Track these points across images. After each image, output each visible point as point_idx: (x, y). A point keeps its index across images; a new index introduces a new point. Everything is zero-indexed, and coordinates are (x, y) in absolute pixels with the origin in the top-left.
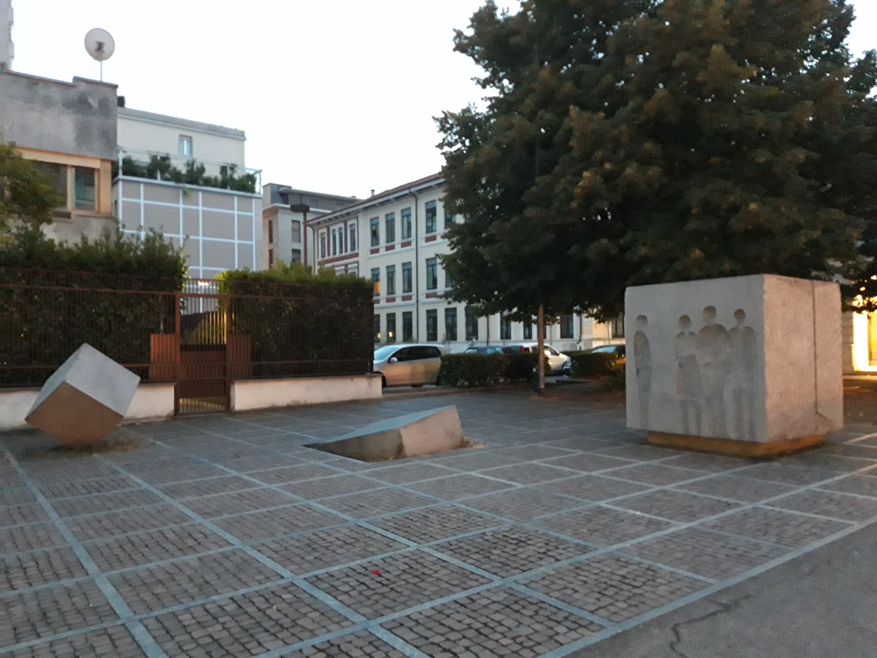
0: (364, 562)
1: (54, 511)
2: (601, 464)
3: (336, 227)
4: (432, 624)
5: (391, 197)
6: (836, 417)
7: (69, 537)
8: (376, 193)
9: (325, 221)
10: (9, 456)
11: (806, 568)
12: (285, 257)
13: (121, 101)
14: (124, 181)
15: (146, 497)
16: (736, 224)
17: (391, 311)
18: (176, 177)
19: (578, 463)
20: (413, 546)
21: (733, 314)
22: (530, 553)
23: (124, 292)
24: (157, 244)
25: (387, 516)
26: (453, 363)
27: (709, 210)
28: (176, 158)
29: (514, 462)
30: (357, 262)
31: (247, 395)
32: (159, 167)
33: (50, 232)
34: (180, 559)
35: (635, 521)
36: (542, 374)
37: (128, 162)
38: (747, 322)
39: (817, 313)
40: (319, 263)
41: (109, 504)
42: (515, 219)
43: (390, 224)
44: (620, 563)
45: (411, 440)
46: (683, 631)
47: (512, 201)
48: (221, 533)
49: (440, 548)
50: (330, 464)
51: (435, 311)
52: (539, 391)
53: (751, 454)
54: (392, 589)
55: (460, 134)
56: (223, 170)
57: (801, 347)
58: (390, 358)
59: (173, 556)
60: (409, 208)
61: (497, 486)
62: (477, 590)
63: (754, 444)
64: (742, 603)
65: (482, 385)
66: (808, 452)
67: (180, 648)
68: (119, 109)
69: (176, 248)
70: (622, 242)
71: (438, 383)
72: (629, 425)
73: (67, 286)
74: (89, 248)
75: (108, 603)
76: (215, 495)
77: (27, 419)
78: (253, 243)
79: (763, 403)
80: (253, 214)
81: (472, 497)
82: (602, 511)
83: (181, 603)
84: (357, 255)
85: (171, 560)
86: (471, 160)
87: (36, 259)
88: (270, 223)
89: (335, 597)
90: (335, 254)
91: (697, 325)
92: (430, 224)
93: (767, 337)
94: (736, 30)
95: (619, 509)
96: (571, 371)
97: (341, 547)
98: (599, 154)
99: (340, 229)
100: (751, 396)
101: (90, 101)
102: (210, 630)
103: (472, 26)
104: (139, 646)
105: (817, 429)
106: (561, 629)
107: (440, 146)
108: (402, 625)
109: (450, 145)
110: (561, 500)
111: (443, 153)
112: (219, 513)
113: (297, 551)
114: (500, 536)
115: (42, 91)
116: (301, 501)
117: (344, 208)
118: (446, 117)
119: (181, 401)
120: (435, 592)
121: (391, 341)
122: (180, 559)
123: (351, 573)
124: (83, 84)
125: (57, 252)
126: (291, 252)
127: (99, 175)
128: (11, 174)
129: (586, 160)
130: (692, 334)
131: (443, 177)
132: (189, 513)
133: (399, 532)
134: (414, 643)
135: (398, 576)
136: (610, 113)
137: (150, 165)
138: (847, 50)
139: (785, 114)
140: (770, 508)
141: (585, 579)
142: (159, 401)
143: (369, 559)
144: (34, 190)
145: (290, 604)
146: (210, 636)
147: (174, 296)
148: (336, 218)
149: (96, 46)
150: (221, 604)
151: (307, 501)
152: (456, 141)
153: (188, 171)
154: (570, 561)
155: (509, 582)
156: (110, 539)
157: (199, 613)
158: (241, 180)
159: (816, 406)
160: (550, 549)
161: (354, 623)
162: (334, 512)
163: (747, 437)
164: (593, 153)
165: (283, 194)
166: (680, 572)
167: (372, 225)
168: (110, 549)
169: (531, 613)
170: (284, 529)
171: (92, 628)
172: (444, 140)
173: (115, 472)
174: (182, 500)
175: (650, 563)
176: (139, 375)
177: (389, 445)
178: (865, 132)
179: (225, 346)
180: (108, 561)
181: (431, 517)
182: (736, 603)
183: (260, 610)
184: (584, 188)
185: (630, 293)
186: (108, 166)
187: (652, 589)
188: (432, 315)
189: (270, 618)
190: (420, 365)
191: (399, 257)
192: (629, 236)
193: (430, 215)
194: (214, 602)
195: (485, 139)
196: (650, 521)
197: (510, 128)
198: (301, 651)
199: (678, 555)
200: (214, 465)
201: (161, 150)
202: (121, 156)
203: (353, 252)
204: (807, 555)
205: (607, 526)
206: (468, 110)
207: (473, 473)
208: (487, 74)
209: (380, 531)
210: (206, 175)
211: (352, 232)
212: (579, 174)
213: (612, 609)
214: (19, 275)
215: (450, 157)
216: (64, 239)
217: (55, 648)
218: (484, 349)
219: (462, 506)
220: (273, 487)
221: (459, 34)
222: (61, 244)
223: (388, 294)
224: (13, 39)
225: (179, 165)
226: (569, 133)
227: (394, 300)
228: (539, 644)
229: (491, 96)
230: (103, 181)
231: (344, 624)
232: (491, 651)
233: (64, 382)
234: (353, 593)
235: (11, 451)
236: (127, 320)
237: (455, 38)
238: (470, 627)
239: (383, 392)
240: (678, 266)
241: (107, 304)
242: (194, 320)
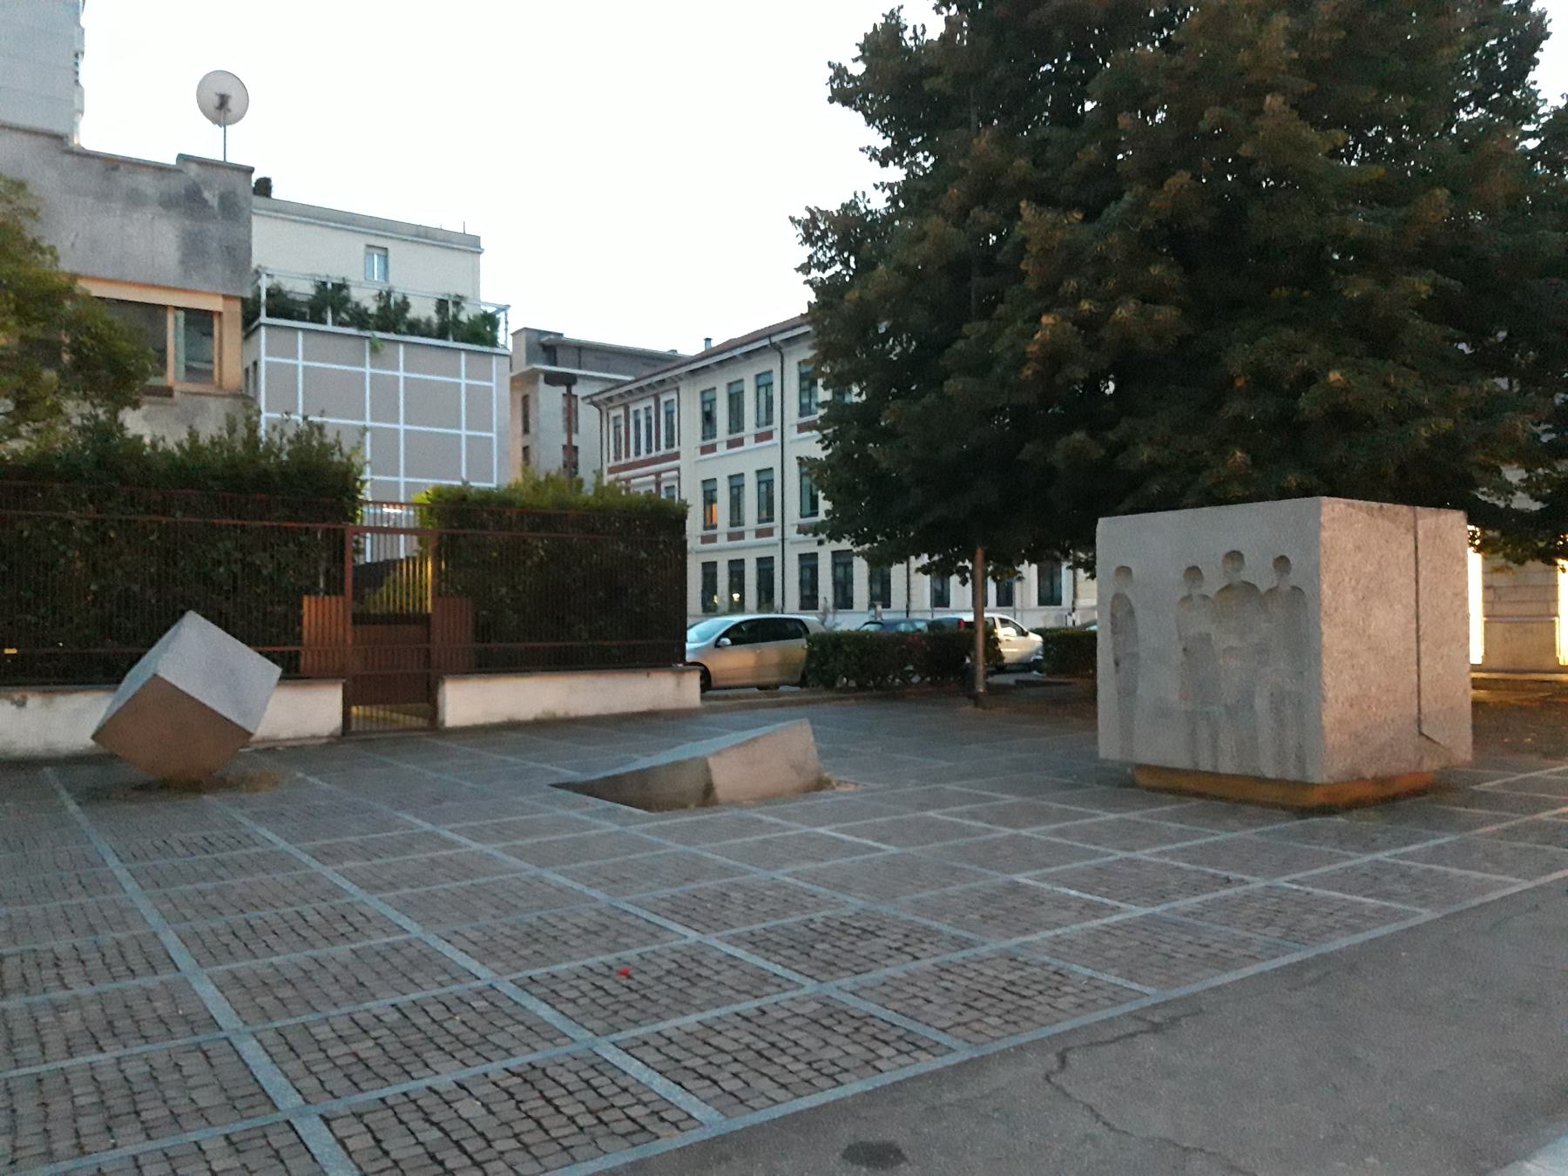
0: (609, 958)
1: (131, 878)
2: (1042, 816)
3: (641, 406)
4: (692, 1043)
5: (737, 352)
6: (1459, 742)
7: (154, 919)
8: (714, 344)
9: (621, 396)
10: (65, 796)
11: (1310, 975)
12: (550, 460)
13: (264, 187)
14: (268, 326)
15: (284, 862)
16: (1308, 404)
17: (764, 553)
18: (360, 319)
19: (1004, 817)
20: (693, 936)
21: (1271, 565)
22: (874, 949)
23: (258, 523)
24: (315, 443)
25: (665, 892)
26: (830, 647)
27: (1263, 380)
28: (359, 286)
29: (897, 813)
30: (678, 469)
31: (467, 701)
32: (329, 301)
33: (137, 423)
34: (323, 951)
35: (1063, 904)
36: (980, 668)
37: (275, 294)
38: (1293, 579)
39: (1422, 562)
40: (611, 471)
41: (221, 872)
42: (930, 398)
43: (735, 400)
44: (1014, 964)
45: (726, 775)
46: (1073, 1058)
47: (921, 369)
48: (392, 914)
49: (736, 940)
50: (590, 814)
51: (715, 564)
52: (975, 699)
53: (1300, 803)
54: (644, 996)
55: (841, 246)
56: (442, 305)
57: (1389, 621)
58: (718, 640)
59: (313, 946)
60: (770, 372)
61: (855, 850)
62: (776, 998)
63: (1305, 786)
64: (1183, 1022)
65: (878, 687)
66: (1399, 799)
67: (308, 1069)
68: (258, 200)
69: (346, 449)
70: (1111, 436)
71: (803, 683)
72: (1102, 755)
73: (163, 514)
74: (201, 449)
75: (206, 1009)
76: (392, 859)
77: (94, 737)
78: (494, 435)
80: (493, 384)
81: (809, 866)
82: (1015, 888)
83: (314, 1009)
84: (676, 456)
85: (309, 952)
86: (853, 295)
87: (113, 468)
88: (525, 399)
89: (553, 1007)
90: (638, 453)
91: (1213, 583)
92: (806, 401)
93: (1326, 603)
94: (1311, 68)
95: (1046, 886)
96: (1045, 665)
97: (578, 937)
98: (1072, 284)
99: (647, 409)
100: (1298, 703)
101: (206, 195)
102: (354, 1047)
103: (863, 58)
104: (247, 1066)
106: (886, 1051)
107: (805, 268)
108: (645, 1043)
109: (823, 267)
110: (954, 870)
111: (810, 283)
112: (393, 886)
113: (508, 942)
114: (836, 924)
115: (125, 180)
116: (532, 870)
117: (654, 371)
118: (814, 219)
119: (354, 710)
120: (709, 1001)
121: (739, 607)
122: (323, 951)
123: (583, 973)
124: (193, 167)
125: (148, 456)
127: (221, 322)
128: (72, 324)
129: (1050, 295)
130: (1205, 597)
131: (809, 323)
132: (346, 885)
133: (676, 917)
134: (658, 1067)
135: (659, 979)
136: (1091, 215)
137: (315, 297)
138: (1535, 94)
139: (1403, 212)
140: (1295, 887)
141: (949, 985)
142: (317, 710)
143: (618, 955)
144: (112, 351)
145: (481, 1014)
146: (355, 1054)
147: (342, 530)
148: (641, 389)
149: (216, 101)
150: (377, 1012)
151: (539, 871)
152: (832, 259)
153: (380, 309)
154: (934, 960)
155: (830, 989)
156: (218, 924)
157: (345, 1028)
158: (473, 323)
159: (1419, 722)
160: (911, 941)
161: (573, 1040)
162: (577, 886)
163: (1292, 774)
164: (1060, 283)
165: (548, 347)
166: (1105, 977)
167: (703, 403)
168: (217, 935)
169: (848, 1030)
170: (493, 911)
171: (179, 1042)
172: (811, 257)
173: (236, 824)
174: (340, 867)
175: (1062, 963)
176: (282, 666)
177: (689, 783)
178: (1551, 240)
179: (428, 617)
180: (208, 951)
181: (733, 894)
182: (1174, 1020)
183: (434, 1021)
184: (1043, 345)
186: (237, 307)
187: (1051, 1000)
188: (808, 563)
189: (448, 1032)
190: (771, 651)
191: (750, 459)
192: (1125, 424)
193: (806, 384)
194: (368, 1010)
195: (882, 255)
196: (1088, 905)
197: (922, 237)
198: (486, 1075)
199: (1113, 953)
200: (399, 814)
201: (333, 272)
202: (264, 283)
203: (670, 451)
204: (1323, 958)
205: (1012, 909)
206: (850, 206)
207: (821, 830)
208: (888, 142)
209: (645, 914)
210: (412, 314)
211: (669, 413)
212: (1036, 319)
213: (977, 1026)
214: (84, 496)
215: (819, 288)
216: (159, 435)
217: (123, 1066)
218: (896, 623)
219: (788, 880)
220: (488, 849)
221: (840, 72)
222: (154, 445)
223: (705, 528)
224: (82, 79)
225: (365, 297)
226: (1021, 247)
227: (741, 536)
228: (847, 1070)
229: (892, 181)
230: (229, 331)
231: (559, 1041)
232: (771, 1079)
233: (155, 675)
234: (581, 1001)
235: (68, 790)
236: (265, 572)
237: (832, 80)
238: (748, 1047)
239: (702, 698)
240: (1206, 480)
241: (229, 544)
242: (380, 572)
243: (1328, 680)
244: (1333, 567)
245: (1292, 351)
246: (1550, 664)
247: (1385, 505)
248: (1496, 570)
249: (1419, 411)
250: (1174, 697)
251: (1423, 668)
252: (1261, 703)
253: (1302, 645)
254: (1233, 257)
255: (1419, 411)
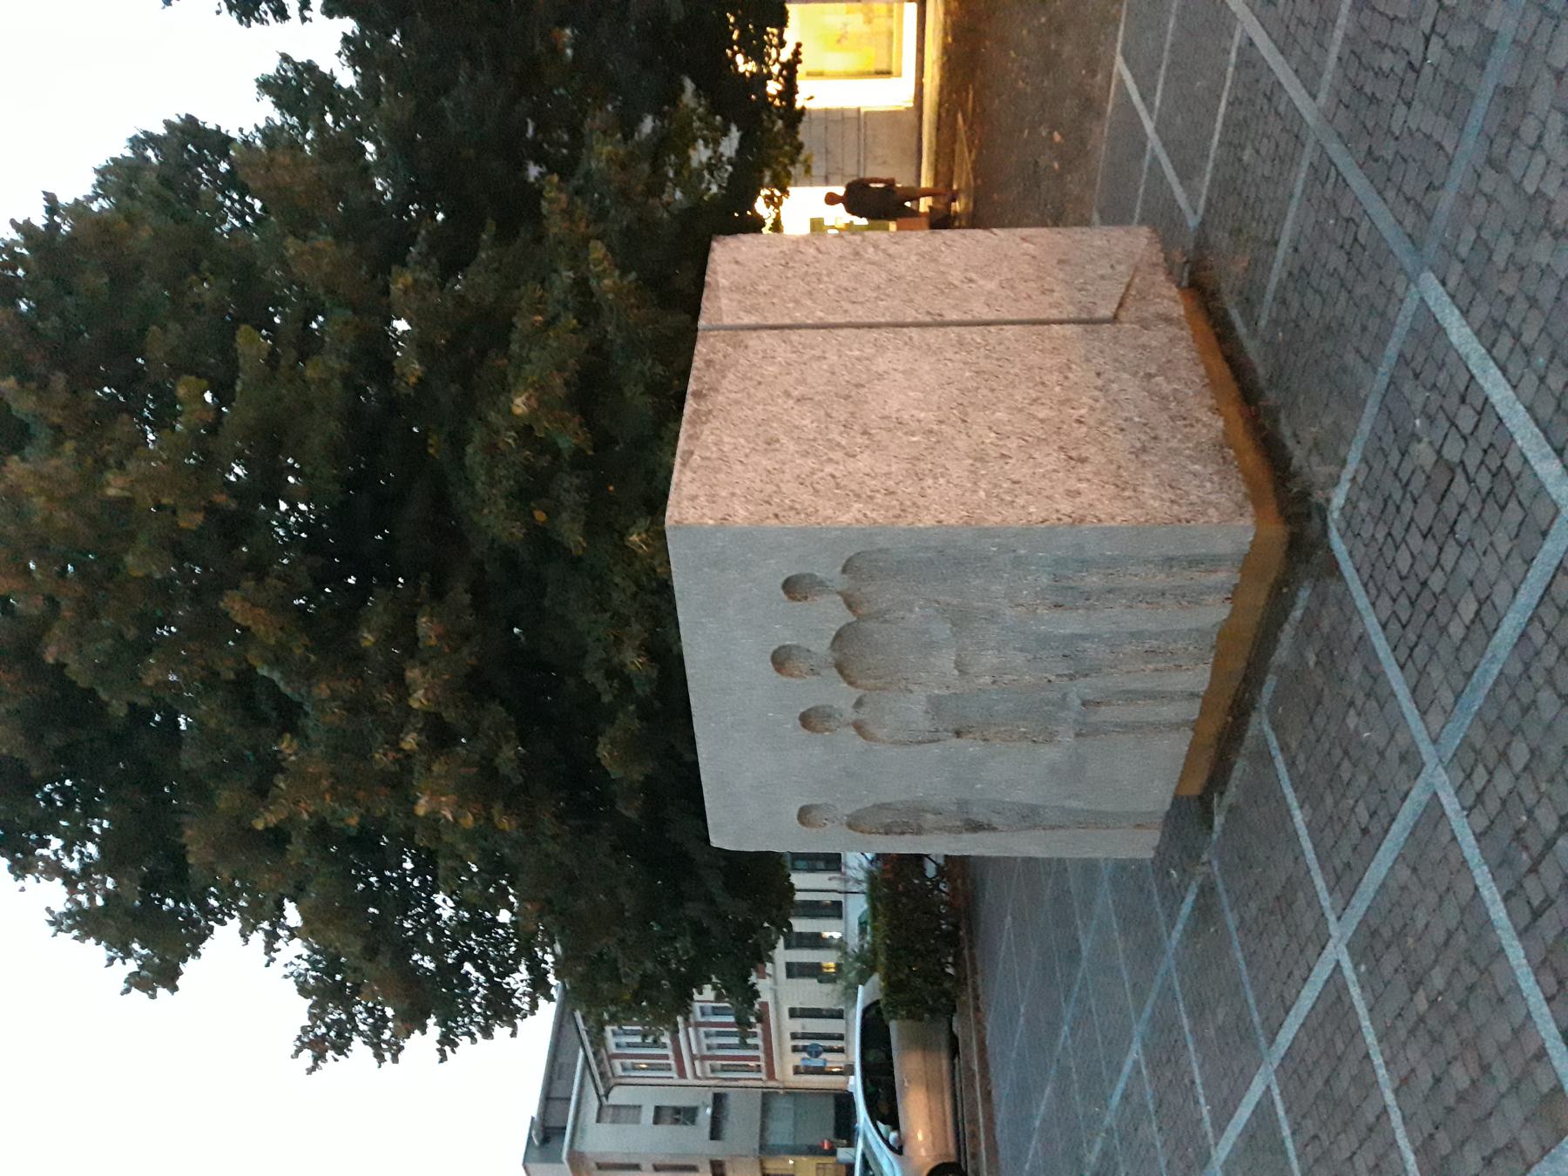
27: (531, 490)
38: (827, 569)
39: (799, 316)
40: (682, 1073)
58: (890, 1147)
66: (1258, 362)
79: (1108, 534)
91: (838, 695)
100: (1072, 568)
105: (1168, 320)
126: (659, 1127)
130: (859, 704)
136: (289, 716)
185: (724, 835)
221: (136, 982)
243: (1036, 511)
244: (806, 497)
245: (491, 449)
246: (913, 118)
247: (692, 386)
248: (808, 170)
249: (581, 285)
250: (1050, 754)
251: (991, 316)
252: (1071, 623)
253: (950, 559)
254: (389, 502)
255: (581, 285)
